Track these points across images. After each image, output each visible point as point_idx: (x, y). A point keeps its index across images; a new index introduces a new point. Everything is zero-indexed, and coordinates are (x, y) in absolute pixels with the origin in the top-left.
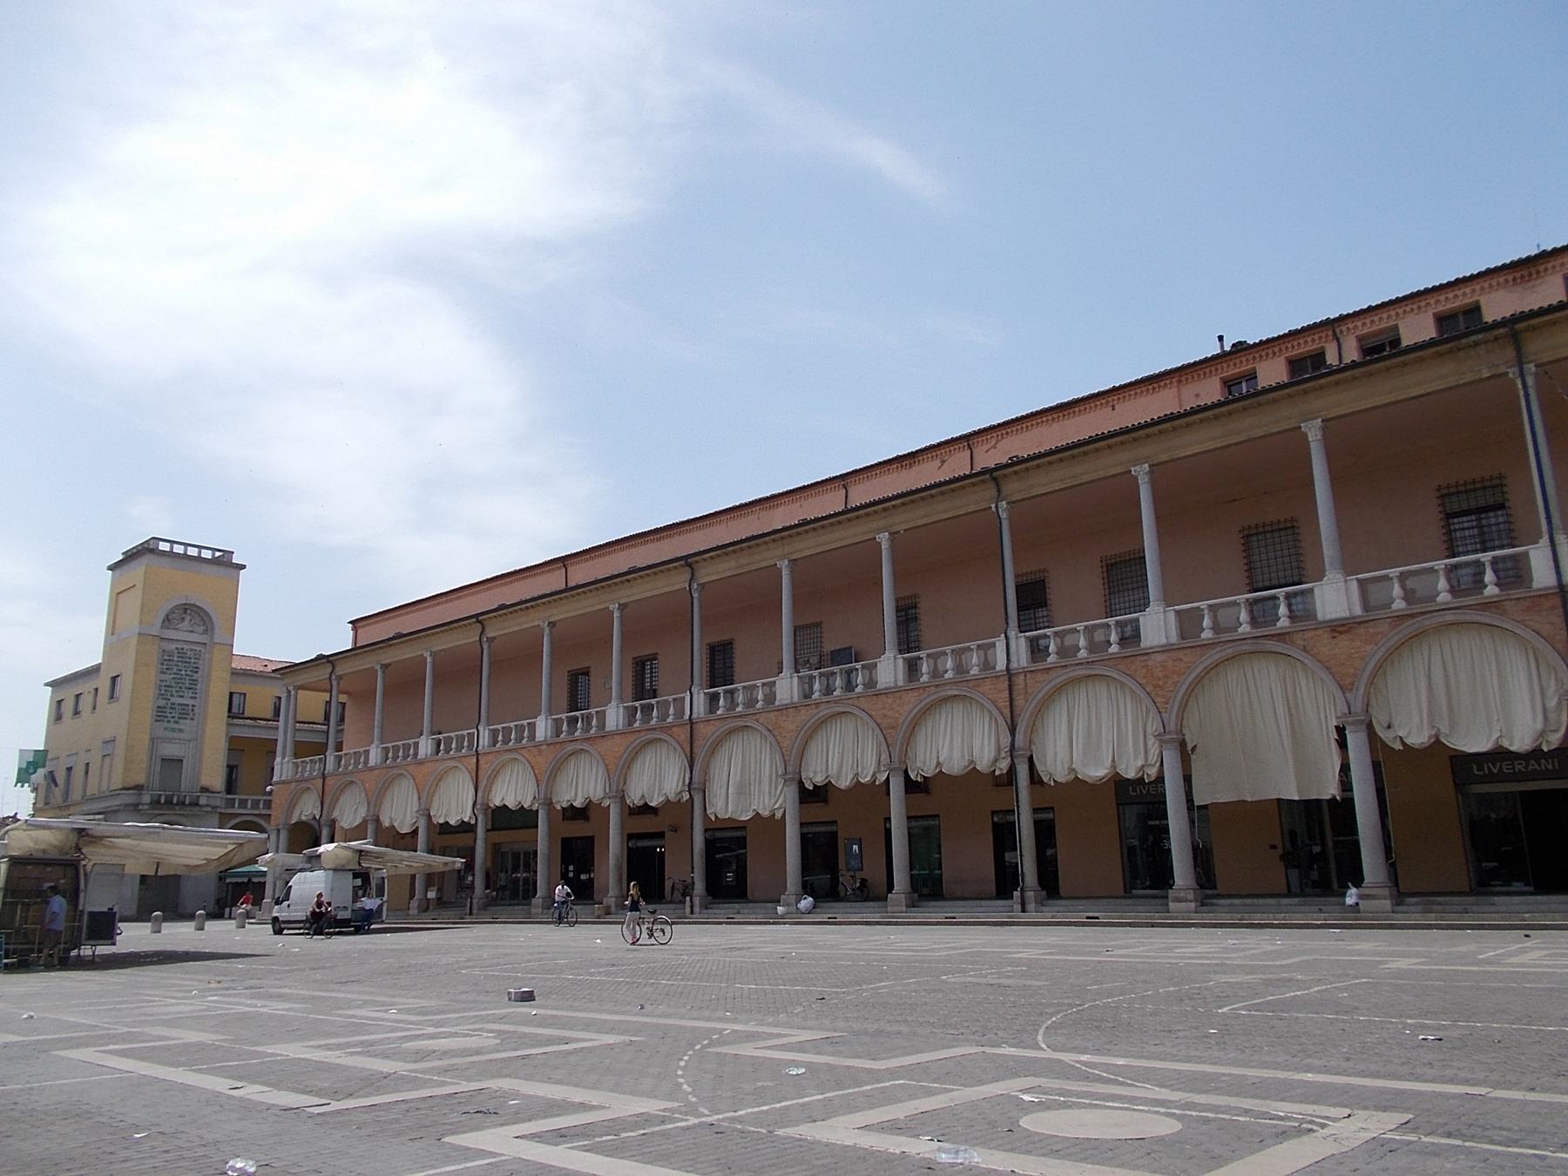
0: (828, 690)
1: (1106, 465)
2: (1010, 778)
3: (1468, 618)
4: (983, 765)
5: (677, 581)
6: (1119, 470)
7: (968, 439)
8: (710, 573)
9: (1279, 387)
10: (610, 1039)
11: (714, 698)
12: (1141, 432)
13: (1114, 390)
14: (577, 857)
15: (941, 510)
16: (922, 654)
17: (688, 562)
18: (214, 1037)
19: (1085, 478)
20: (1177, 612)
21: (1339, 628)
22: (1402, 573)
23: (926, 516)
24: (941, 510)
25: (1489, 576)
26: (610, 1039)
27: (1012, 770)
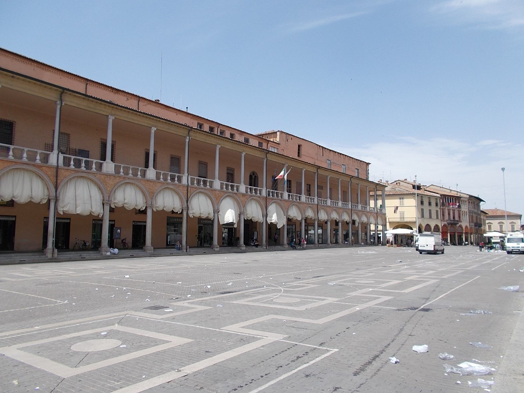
0: (126, 173)
1: (145, 122)
2: (144, 212)
3: (20, 167)
4: (36, 200)
5: (51, 96)
6: (105, 114)
7: (139, 98)
8: (69, 101)
9: (205, 132)
10: (313, 286)
11: (289, 195)
12: (91, 99)
13: (179, 110)
14: (139, 231)
15: (173, 130)
16: (12, 147)
17: (64, 90)
18: (336, 299)
19: (208, 142)
20: (64, 157)
21: (108, 175)
22: (15, 148)
23: (168, 129)
24: (173, 130)
25: (72, 163)
26: (313, 286)
27: (182, 213)
